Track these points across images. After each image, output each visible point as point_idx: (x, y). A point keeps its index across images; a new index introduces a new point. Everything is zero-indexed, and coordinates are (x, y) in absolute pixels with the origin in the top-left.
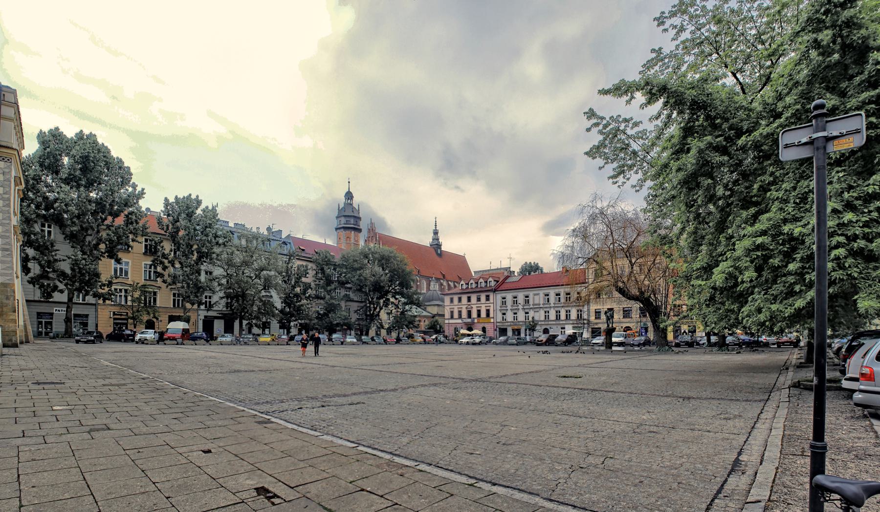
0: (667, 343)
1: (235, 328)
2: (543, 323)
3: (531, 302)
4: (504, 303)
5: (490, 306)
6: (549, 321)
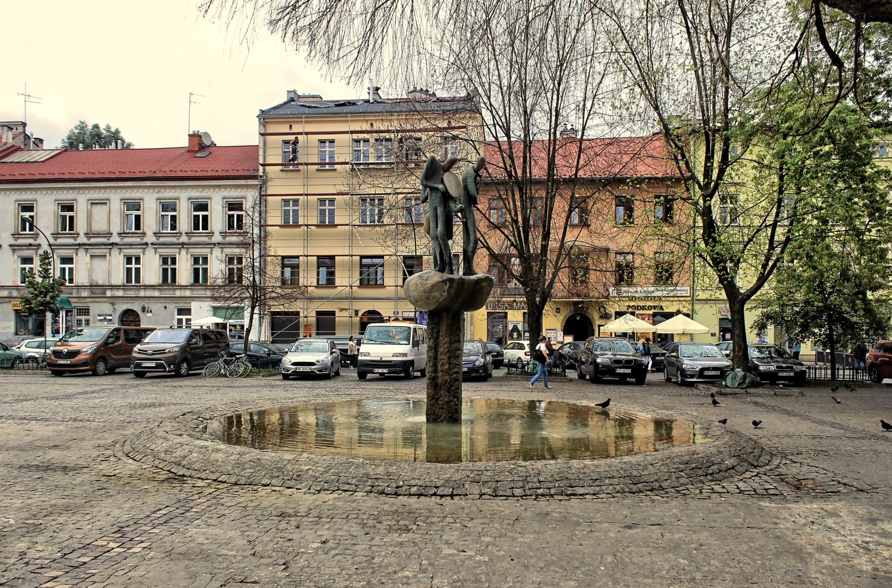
2: (120, 293)
6: (139, 288)
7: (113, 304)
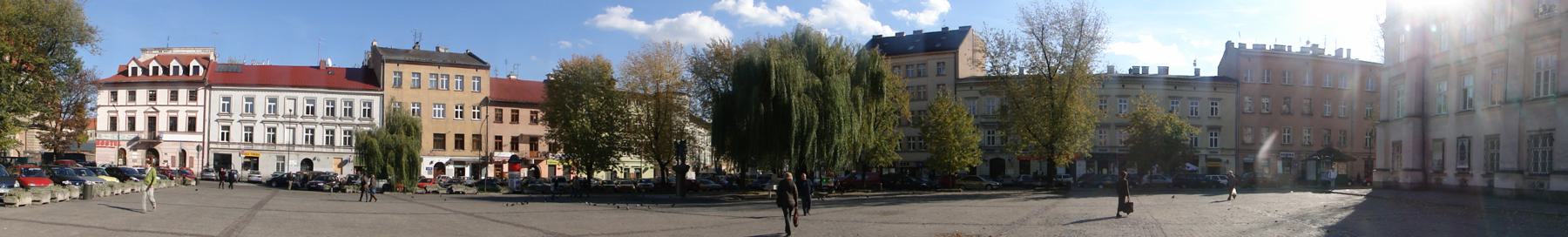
0: (231, 179)
1: (1220, 196)
2: (304, 149)
3: (280, 112)
4: (227, 108)
5: (196, 112)
6: (229, 144)
7: (298, 155)
